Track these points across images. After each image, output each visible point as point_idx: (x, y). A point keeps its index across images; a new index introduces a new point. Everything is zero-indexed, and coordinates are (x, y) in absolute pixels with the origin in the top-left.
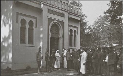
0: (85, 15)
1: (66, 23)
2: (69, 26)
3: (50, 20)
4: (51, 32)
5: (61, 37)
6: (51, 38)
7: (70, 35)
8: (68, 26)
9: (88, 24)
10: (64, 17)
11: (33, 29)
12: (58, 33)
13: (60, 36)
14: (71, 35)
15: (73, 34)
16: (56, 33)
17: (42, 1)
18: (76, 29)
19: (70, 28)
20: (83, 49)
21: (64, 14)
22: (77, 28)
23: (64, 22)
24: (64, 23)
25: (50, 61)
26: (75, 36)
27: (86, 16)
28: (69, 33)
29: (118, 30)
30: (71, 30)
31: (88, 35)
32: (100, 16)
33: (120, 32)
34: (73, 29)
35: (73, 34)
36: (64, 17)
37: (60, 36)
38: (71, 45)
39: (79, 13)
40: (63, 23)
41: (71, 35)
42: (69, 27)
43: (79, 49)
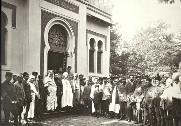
0: (118, 23)
1: (83, 26)
2: (88, 31)
3: (46, 16)
4: (49, 40)
5: (71, 53)
6: (50, 53)
7: (90, 50)
8: (87, 33)
9: (122, 37)
10: (77, 12)
11: (7, 31)
12: (65, 45)
13: (70, 49)
14: (92, 52)
15: (96, 48)
16: (62, 43)
17: (142, 118)
18: (103, 40)
19: (90, 36)
20: (147, 80)
21: (78, 8)
22: (105, 37)
23: (77, 23)
24: (79, 24)
25: (11, 112)
26: (100, 53)
27: (121, 25)
28: (89, 47)
29: (169, 50)
30: (92, 41)
31: (125, 57)
32: (142, 29)
33: (171, 54)
34: (97, 39)
35: (96, 48)
36: (77, 12)
37: (69, 51)
38: (91, 69)
39: (109, 10)
40: (75, 25)
41: (92, 49)
42: (89, 35)
43: (13, 74)
